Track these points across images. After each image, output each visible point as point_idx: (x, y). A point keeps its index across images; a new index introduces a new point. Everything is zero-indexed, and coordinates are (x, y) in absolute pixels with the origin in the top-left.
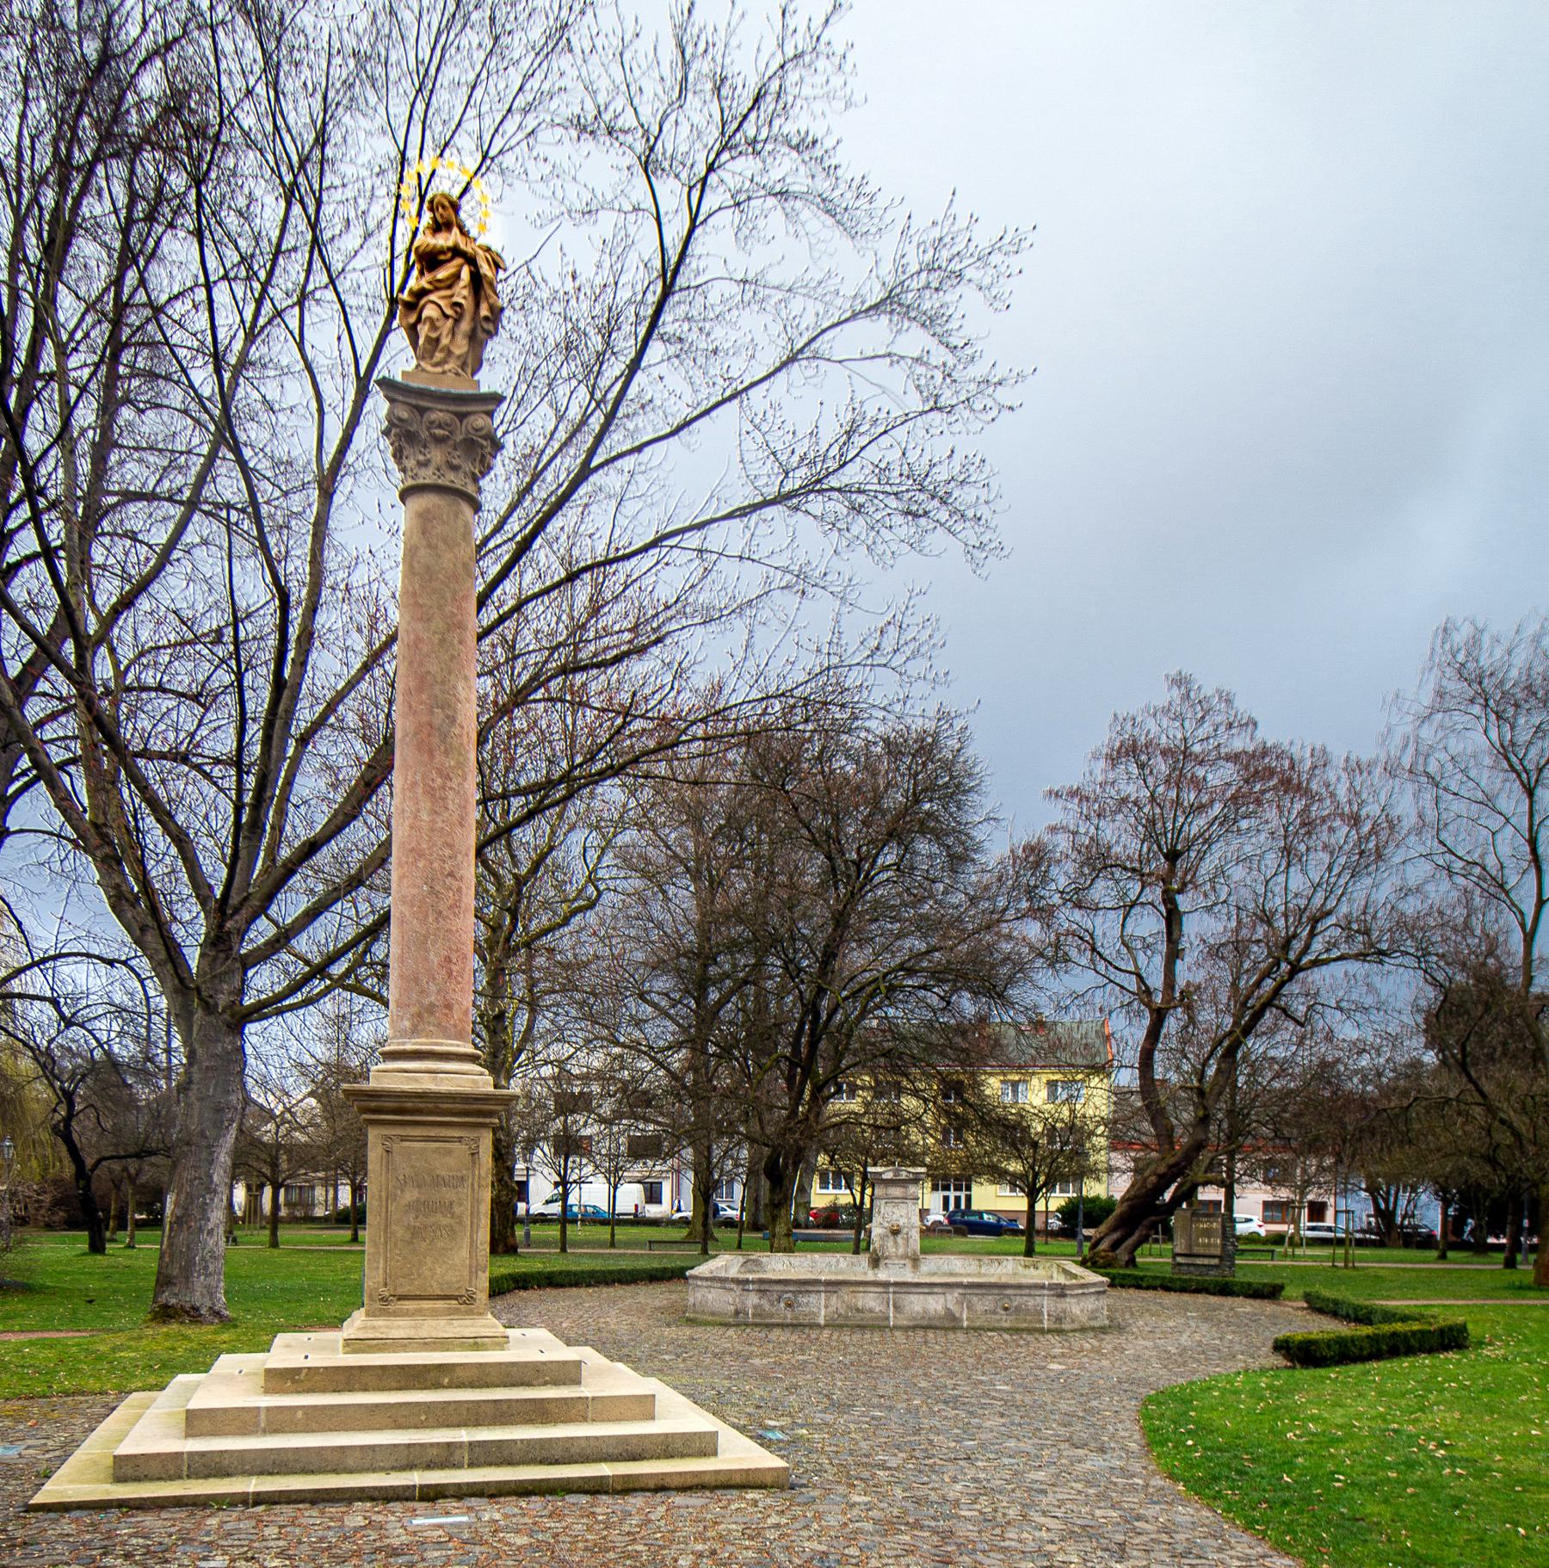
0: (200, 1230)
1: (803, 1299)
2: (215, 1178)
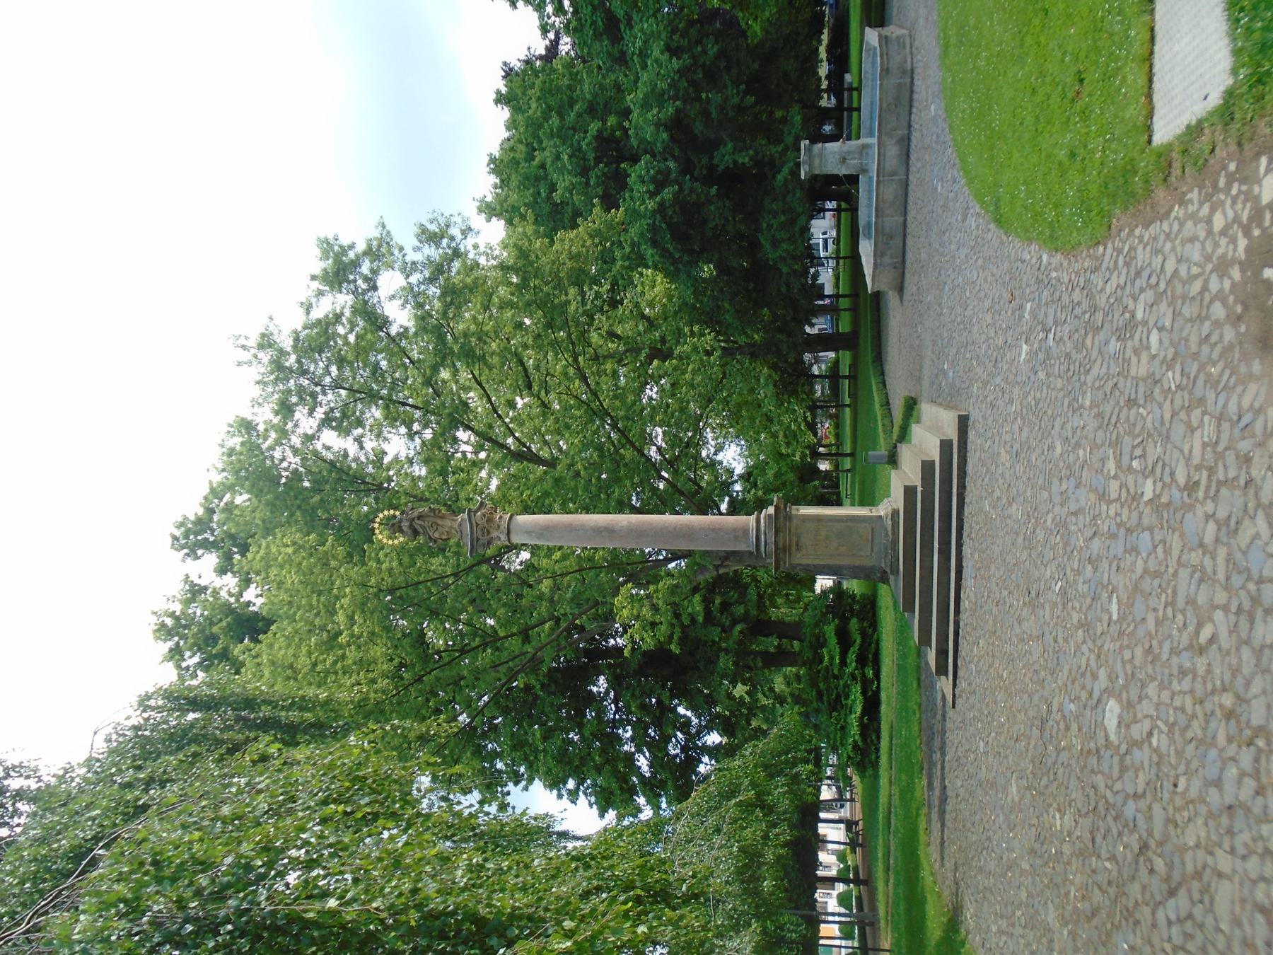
1: (887, 230)
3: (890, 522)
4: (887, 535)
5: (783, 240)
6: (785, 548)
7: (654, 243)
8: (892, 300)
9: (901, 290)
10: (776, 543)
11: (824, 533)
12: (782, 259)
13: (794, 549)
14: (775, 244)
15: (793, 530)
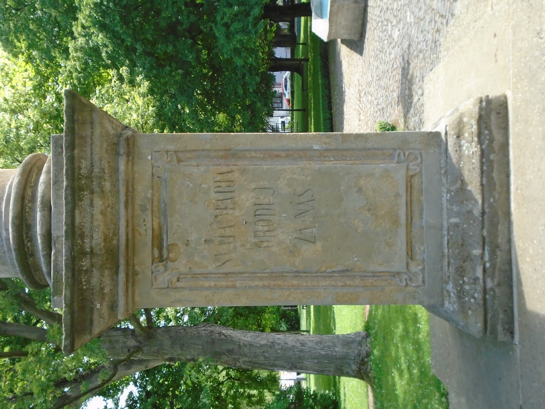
0: (301, 351)
2: (263, 342)
3: (470, 149)
4: (461, 193)
5: (237, 33)
6: (112, 254)
7: (103, 27)
8: (344, 51)
9: (357, 44)
10: (74, 233)
11: (246, 199)
12: (237, 51)
13: (145, 255)
14: (228, 36)
15: (143, 191)
